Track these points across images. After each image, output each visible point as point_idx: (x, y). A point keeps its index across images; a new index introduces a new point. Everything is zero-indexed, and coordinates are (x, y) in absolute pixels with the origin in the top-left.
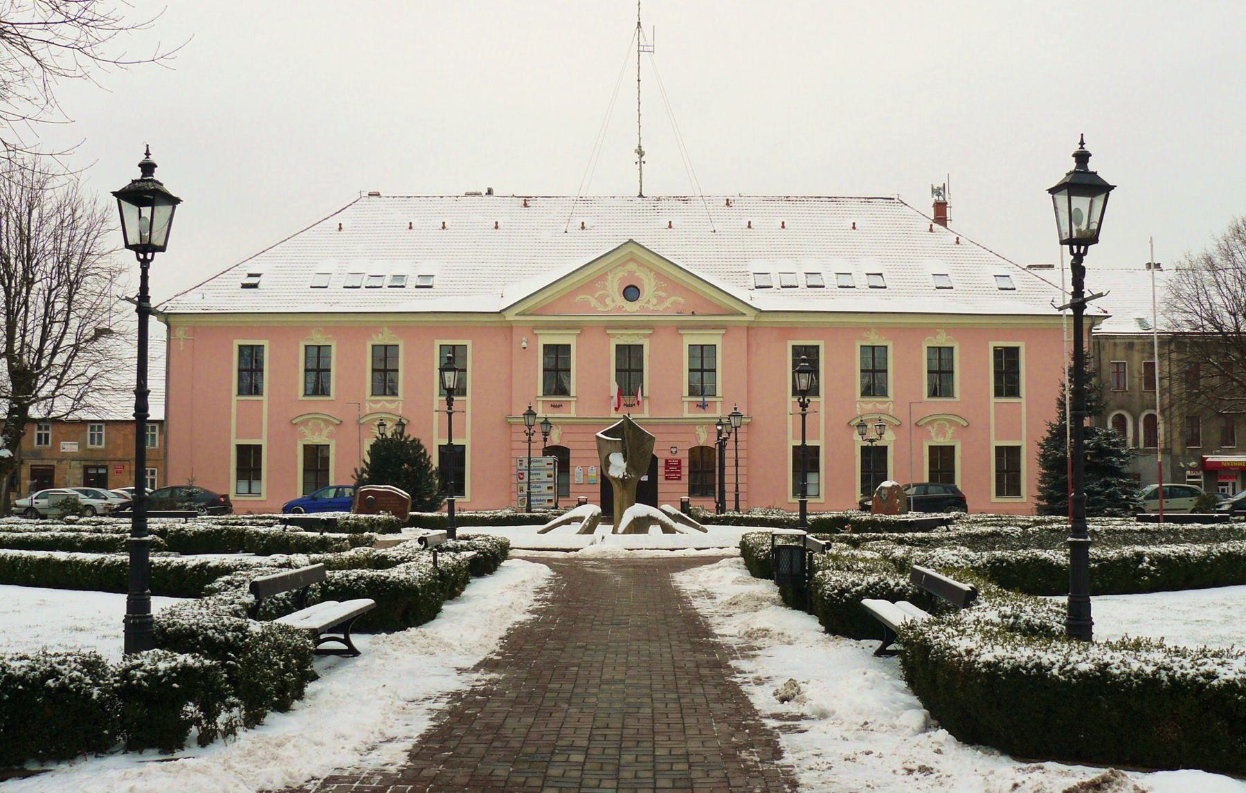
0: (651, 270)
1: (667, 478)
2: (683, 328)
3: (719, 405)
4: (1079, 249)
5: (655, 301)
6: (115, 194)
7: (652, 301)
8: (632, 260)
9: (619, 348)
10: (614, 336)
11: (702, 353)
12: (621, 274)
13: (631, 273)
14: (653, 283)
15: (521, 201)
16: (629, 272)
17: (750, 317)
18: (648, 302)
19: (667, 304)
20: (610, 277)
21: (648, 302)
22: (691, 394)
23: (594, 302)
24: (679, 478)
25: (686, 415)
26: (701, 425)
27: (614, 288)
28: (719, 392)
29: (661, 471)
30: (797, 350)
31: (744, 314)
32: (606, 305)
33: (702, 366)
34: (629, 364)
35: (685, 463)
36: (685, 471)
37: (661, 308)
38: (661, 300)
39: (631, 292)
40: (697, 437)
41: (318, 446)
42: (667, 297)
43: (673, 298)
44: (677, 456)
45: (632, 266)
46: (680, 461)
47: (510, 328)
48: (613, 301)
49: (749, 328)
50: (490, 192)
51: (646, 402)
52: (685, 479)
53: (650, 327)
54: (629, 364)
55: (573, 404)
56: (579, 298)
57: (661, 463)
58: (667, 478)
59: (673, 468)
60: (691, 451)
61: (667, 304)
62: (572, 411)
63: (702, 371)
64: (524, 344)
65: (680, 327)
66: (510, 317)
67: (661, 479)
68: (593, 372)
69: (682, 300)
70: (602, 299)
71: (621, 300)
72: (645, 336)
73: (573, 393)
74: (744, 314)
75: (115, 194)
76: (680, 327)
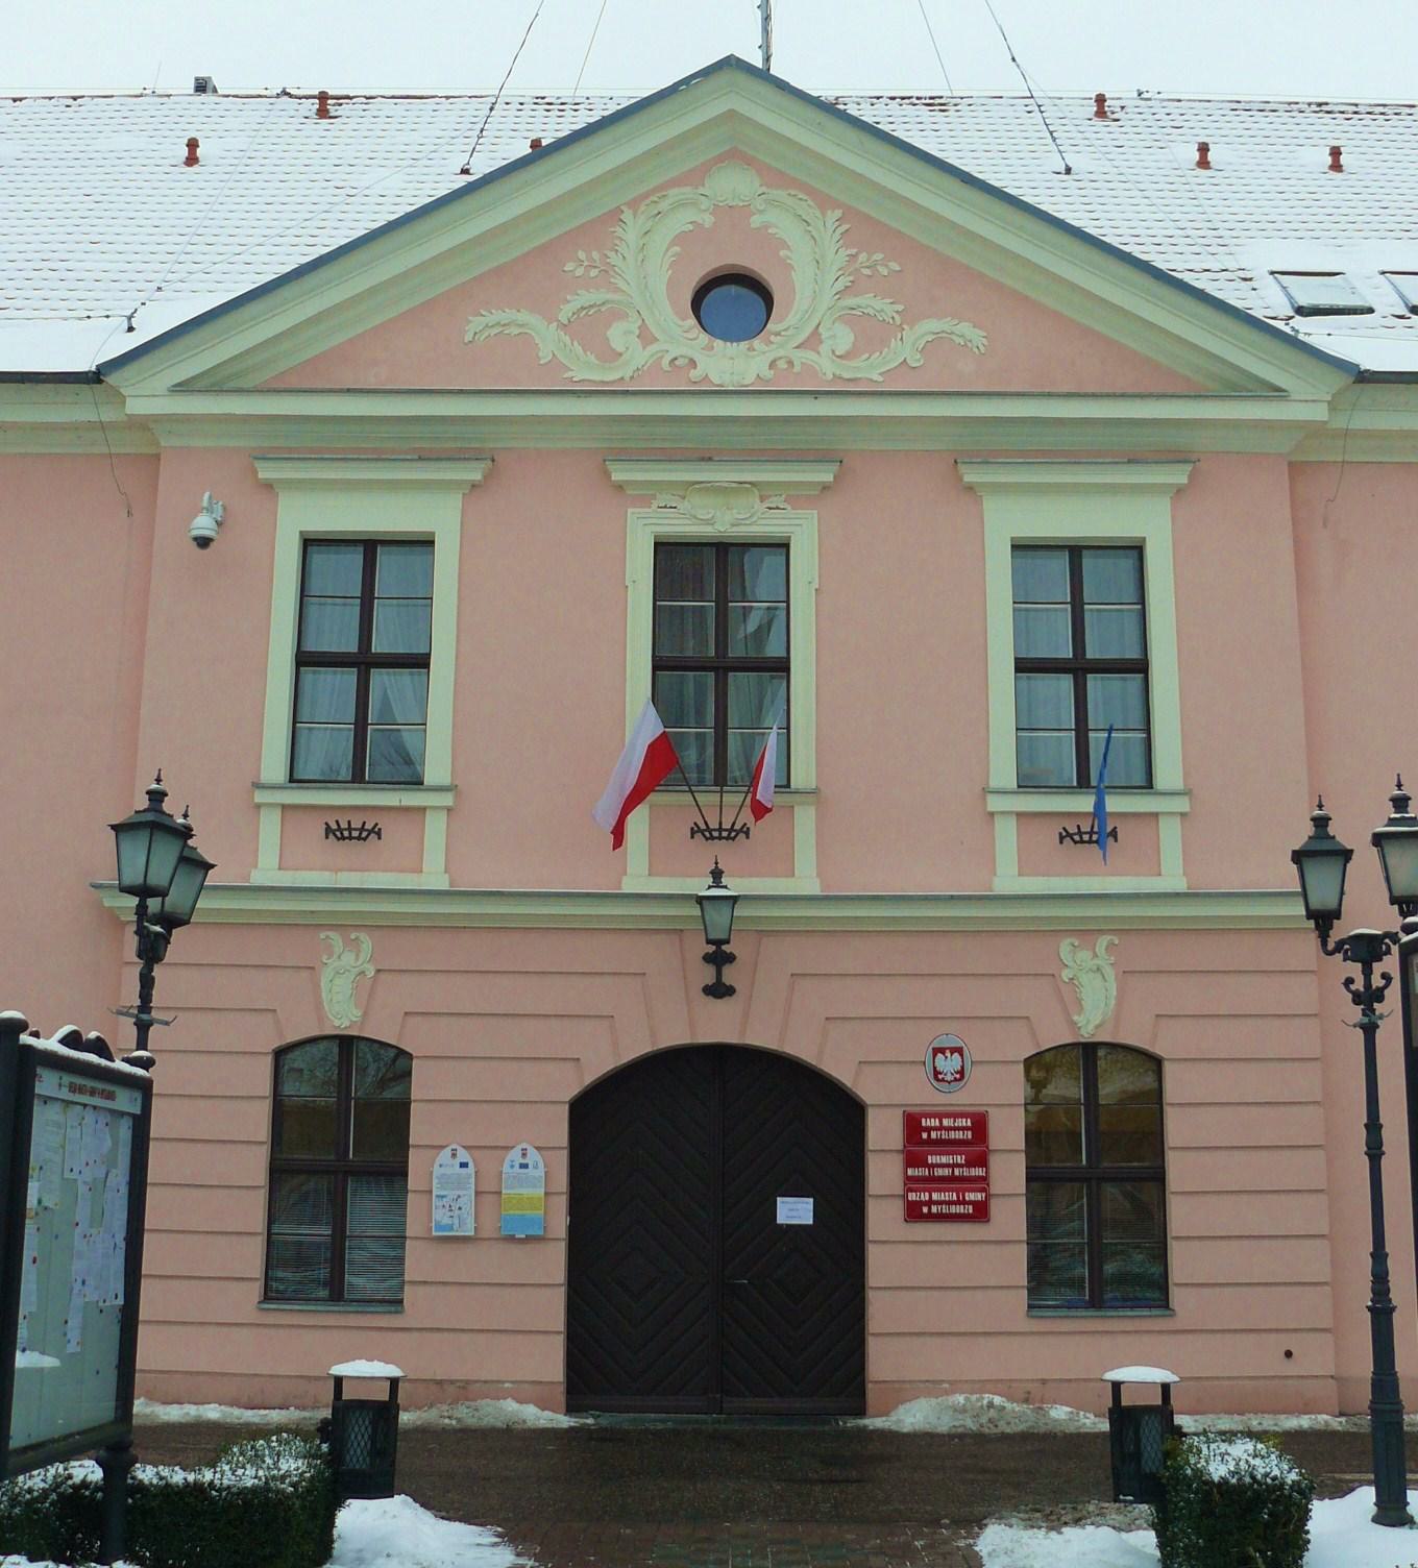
0: (824, 202)
1: (914, 1213)
2: (987, 459)
3: (1170, 835)
4: (1408, 907)
5: (844, 339)
6: (113, 827)
7: (822, 329)
8: (735, 156)
9: (667, 552)
10: (644, 495)
11: (367, 568)
12: (680, 222)
13: (732, 215)
14: (836, 258)
15: (315, 104)
16: (720, 211)
17: (1307, 403)
18: (813, 341)
19: (906, 348)
20: (631, 230)
21: (813, 341)
22: (1027, 783)
23: (549, 341)
24: (981, 1213)
25: (1008, 879)
26: (1085, 933)
27: (651, 270)
28: (1168, 770)
29: (884, 1174)
30: (678, 562)
31: (1277, 393)
32: (611, 356)
33: (1086, 653)
34: (714, 623)
35: (1009, 1134)
36: (1009, 1173)
37: (871, 370)
38: (871, 334)
39: (733, 296)
40: (1068, 999)
41: (407, 1175)
42: (910, 317)
43: (932, 325)
44: (964, 1097)
45: (733, 185)
46: (980, 1125)
47: (140, 460)
48: (646, 337)
49: (1305, 466)
50: (202, 86)
51: (805, 820)
52: (1011, 1216)
53: (811, 444)
54: (714, 623)
55: (435, 829)
56: (477, 325)
57: (883, 1134)
58: (914, 1213)
59: (947, 1156)
60: (1039, 1066)
61: (906, 348)
62: (429, 859)
63: (1079, 668)
64: (203, 524)
65: (969, 455)
66: (146, 396)
67: (882, 1217)
68: (541, 657)
69: (976, 336)
70: (589, 329)
71: (681, 337)
72: (798, 496)
73: (436, 770)
74: (1277, 393)
75: (113, 827)
76: (969, 455)
